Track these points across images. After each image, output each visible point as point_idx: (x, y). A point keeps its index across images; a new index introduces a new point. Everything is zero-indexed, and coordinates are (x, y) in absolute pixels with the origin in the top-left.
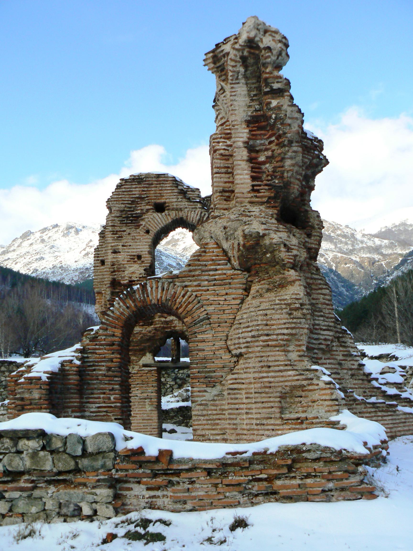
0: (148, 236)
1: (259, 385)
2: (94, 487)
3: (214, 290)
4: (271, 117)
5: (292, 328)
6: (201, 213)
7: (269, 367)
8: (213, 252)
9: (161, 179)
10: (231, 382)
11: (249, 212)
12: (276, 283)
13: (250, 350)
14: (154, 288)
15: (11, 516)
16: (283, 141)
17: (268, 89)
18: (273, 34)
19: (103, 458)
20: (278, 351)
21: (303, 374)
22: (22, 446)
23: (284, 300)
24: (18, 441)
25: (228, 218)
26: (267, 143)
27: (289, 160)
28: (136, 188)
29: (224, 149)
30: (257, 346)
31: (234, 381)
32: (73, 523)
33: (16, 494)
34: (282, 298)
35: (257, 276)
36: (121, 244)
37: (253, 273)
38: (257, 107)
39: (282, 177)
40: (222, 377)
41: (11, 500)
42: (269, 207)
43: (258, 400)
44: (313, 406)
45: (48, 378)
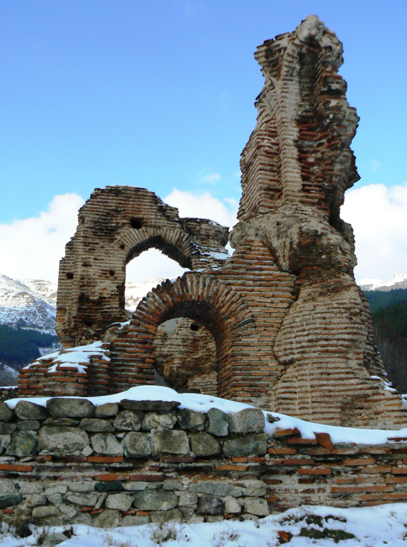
0: (122, 251)
1: (318, 394)
2: (240, 478)
3: (260, 291)
4: (328, 117)
5: (353, 334)
6: (181, 233)
7: (329, 374)
8: (259, 250)
9: (140, 193)
10: (283, 390)
11: (301, 210)
12: (330, 286)
13: (305, 356)
14: (194, 283)
15: (134, 514)
16: (336, 144)
17: (325, 89)
18: (331, 37)
19: (255, 439)
20: (338, 357)
21: (366, 383)
22: (150, 423)
23: (343, 304)
24: (144, 416)
25: (282, 213)
26: (315, 145)
27: (339, 165)
28: (112, 199)
29: (269, 147)
30: (314, 352)
31: (286, 390)
32: (218, 522)
33: (141, 485)
34: (340, 302)
35: (307, 279)
36: (93, 257)
37: (303, 275)
38: (307, 107)
39: (331, 181)
40: (268, 386)
41: (132, 493)
42: (320, 209)
43: (318, 410)
44: (377, 418)
45: (85, 369)
